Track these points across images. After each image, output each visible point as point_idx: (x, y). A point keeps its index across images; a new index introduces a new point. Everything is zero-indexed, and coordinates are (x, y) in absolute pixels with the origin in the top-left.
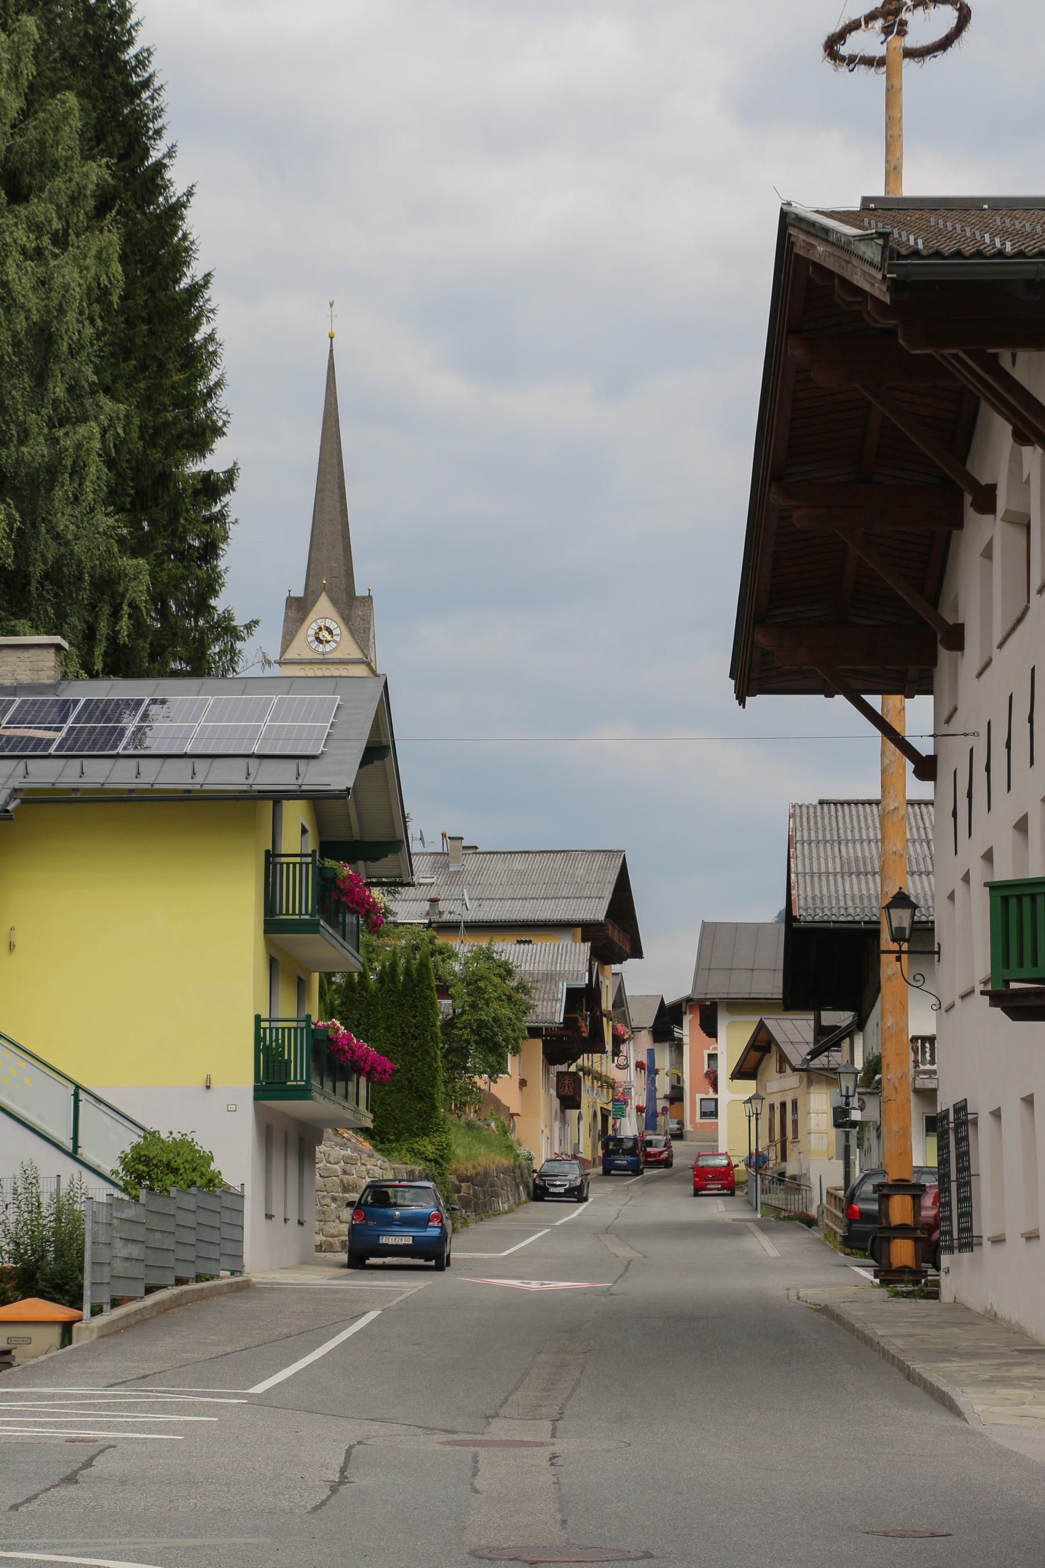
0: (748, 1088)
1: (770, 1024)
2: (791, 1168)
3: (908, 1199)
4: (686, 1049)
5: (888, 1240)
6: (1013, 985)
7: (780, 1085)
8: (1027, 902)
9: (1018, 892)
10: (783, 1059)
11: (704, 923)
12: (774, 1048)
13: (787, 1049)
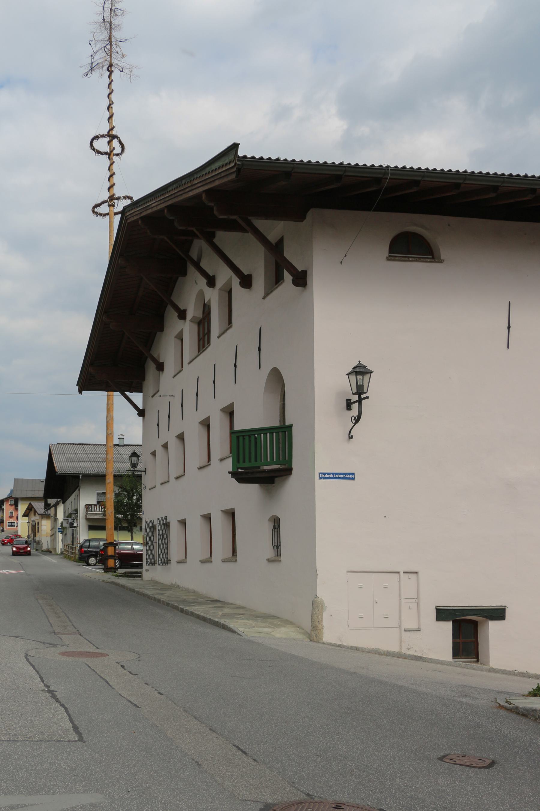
0: (26, 519)
1: (32, 503)
2: (37, 539)
3: (113, 548)
4: (5, 511)
5: (107, 559)
6: (239, 470)
7: (33, 517)
8: (247, 438)
9: (243, 434)
10: (35, 512)
11: (15, 479)
12: (33, 509)
13: (37, 510)
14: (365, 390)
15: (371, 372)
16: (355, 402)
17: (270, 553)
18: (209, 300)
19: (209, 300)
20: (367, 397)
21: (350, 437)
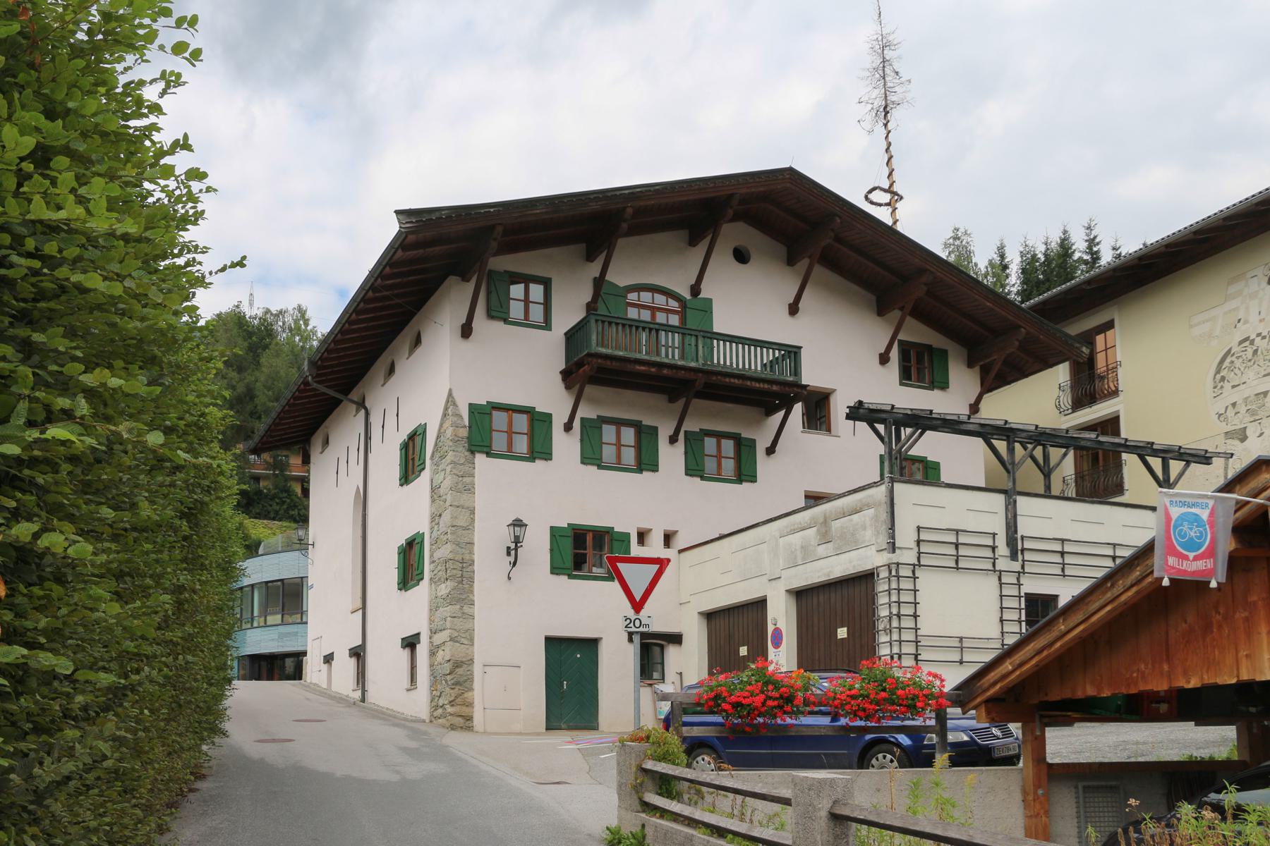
17: (406, 682)
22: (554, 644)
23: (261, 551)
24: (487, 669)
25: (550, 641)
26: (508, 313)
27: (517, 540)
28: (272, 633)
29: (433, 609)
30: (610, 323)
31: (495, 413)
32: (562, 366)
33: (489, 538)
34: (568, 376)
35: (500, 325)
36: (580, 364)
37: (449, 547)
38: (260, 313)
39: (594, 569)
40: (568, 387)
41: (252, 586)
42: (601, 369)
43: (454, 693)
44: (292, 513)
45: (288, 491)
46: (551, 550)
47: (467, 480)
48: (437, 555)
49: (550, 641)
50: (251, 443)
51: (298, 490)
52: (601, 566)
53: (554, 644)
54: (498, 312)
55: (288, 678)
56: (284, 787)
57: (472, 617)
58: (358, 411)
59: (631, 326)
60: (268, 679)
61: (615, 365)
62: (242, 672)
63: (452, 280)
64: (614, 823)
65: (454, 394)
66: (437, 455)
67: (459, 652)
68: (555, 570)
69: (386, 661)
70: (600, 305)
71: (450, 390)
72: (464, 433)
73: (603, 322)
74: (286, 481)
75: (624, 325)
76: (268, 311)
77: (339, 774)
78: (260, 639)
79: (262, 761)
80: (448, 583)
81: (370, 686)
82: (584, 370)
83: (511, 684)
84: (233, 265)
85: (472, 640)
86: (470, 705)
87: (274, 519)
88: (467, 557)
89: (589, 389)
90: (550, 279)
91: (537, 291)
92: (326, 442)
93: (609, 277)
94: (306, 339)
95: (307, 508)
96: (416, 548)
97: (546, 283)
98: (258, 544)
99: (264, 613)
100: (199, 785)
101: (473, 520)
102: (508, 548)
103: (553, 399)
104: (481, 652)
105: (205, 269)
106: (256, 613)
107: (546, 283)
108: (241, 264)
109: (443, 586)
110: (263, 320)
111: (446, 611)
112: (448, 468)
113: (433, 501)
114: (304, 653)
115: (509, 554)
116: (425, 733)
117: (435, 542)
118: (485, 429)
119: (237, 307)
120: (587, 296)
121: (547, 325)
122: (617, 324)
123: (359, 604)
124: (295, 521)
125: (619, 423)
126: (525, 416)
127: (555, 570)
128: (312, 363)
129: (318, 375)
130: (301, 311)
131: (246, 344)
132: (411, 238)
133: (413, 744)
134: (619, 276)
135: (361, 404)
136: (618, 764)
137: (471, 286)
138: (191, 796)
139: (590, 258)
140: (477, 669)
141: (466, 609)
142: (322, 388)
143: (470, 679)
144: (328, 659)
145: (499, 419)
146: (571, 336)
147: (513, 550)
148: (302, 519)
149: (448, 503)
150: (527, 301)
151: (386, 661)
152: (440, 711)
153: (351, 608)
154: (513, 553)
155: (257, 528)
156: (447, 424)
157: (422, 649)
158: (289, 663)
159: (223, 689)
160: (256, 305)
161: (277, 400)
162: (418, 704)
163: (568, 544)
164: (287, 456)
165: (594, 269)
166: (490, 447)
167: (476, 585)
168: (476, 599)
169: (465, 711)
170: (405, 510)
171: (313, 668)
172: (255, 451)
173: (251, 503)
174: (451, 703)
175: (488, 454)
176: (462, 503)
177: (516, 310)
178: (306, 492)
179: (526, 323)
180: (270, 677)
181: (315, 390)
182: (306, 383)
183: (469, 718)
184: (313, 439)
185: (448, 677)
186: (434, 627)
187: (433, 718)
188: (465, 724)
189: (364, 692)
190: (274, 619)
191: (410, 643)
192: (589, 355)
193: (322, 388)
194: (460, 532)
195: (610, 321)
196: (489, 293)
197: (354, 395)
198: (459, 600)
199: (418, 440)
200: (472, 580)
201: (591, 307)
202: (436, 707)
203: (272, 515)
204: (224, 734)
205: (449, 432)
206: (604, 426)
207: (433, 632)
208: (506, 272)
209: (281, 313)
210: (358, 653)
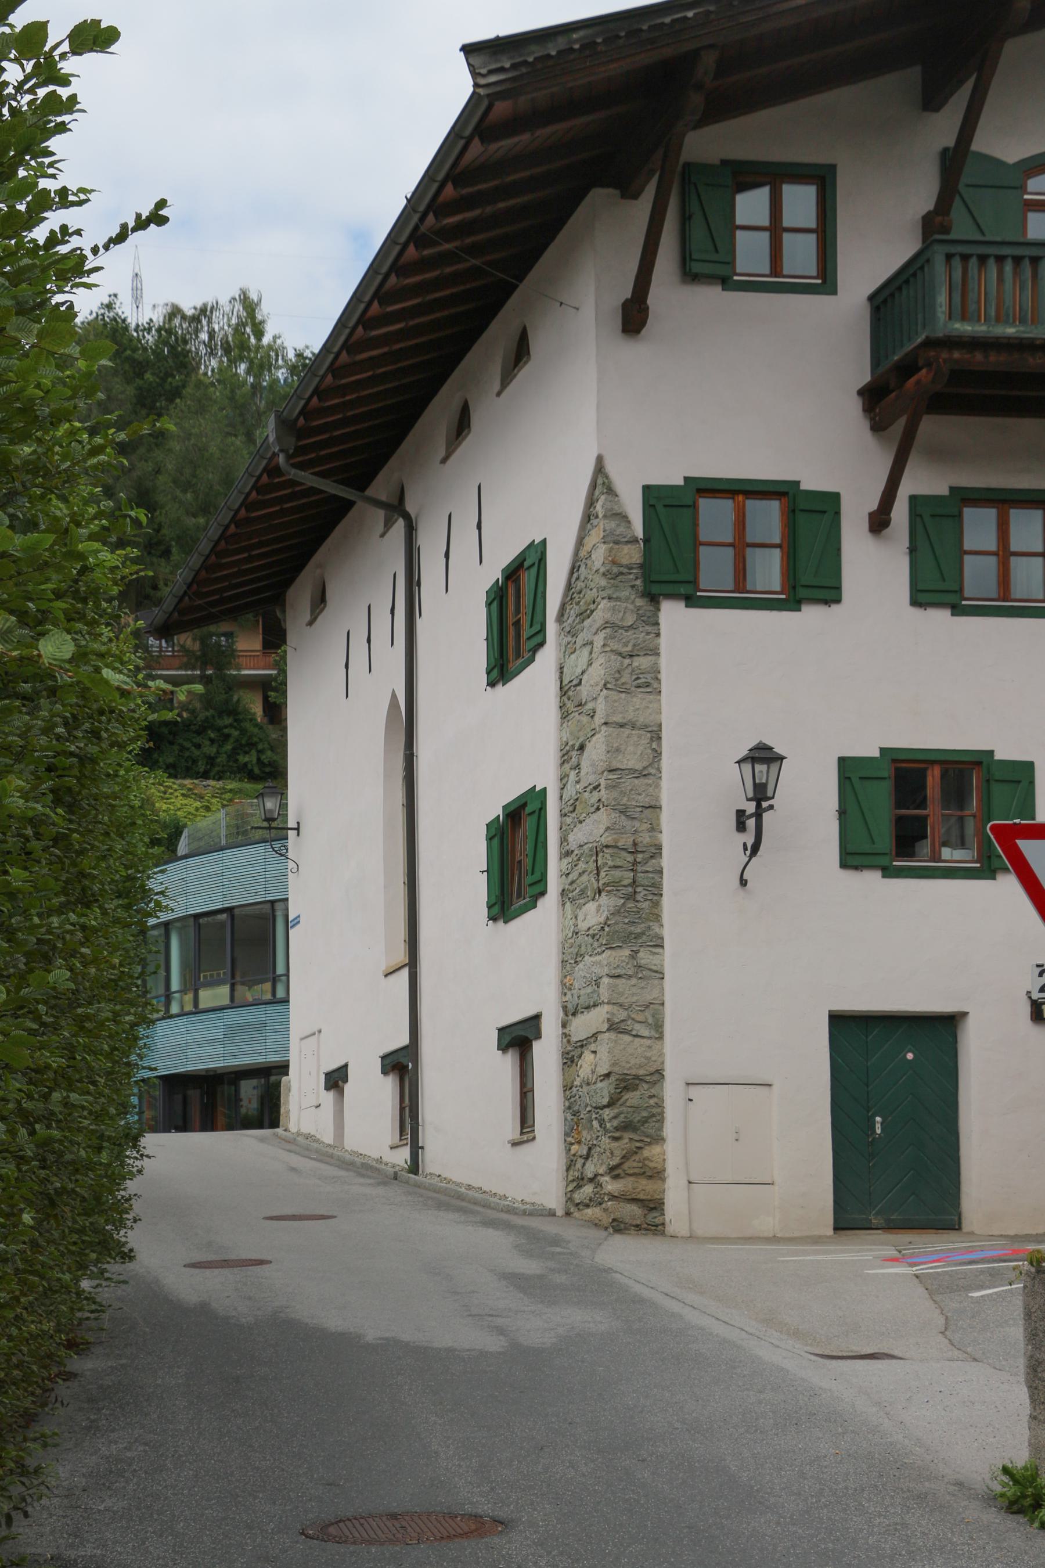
14: (770, 794)
15: (782, 758)
16: (751, 816)
17: (511, 1128)
18: (70, 130)
19: (70, 130)
20: (771, 807)
21: (743, 883)
22: (855, 1034)
23: (182, 848)
24: (694, 1092)
25: (839, 1021)
26: (732, 263)
27: (761, 794)
28: (211, 1027)
29: (570, 958)
30: (983, 259)
31: (703, 503)
32: (860, 372)
33: (693, 793)
34: (875, 398)
35: (711, 295)
36: (907, 368)
37: (603, 817)
38: (158, 317)
39: (946, 853)
40: (878, 427)
41: (167, 925)
42: (958, 375)
43: (619, 1148)
44: (243, 759)
45: (234, 712)
46: (842, 813)
47: (642, 662)
48: (577, 837)
49: (839, 1021)
50: (158, 614)
51: (257, 709)
52: (962, 844)
53: (855, 1034)
54: (709, 265)
55: (247, 1124)
56: (261, 1366)
57: (660, 975)
58: (388, 524)
59: (1017, 260)
60: (204, 1129)
61: (995, 360)
62: (148, 1114)
63: (598, 195)
64: (1020, 1457)
65: (610, 468)
66: (573, 611)
67: (631, 1053)
68: (852, 858)
69: (466, 1083)
70: (958, 213)
71: (600, 460)
72: (633, 555)
73: (965, 258)
74: (229, 689)
75: (1017, 260)
76: (175, 312)
77: (371, 1335)
78: (184, 1042)
79: (203, 1309)
80: (604, 899)
81: (428, 1137)
82: (916, 383)
83: (750, 1127)
84: (142, 224)
85: (658, 1027)
86: (658, 1174)
87: (205, 775)
88: (645, 839)
89: (930, 426)
90: (832, 168)
91: (800, 203)
92: (320, 600)
93: (980, 144)
94: (262, 364)
95: (281, 746)
96: (529, 824)
97: (823, 179)
98: (176, 832)
99: (193, 984)
100: (75, 1363)
101: (657, 754)
102: (741, 813)
103: (828, 449)
104: (680, 1056)
105: (82, 244)
106: (175, 986)
107: (823, 179)
108: (157, 218)
109: (591, 906)
110: (165, 331)
111: (599, 963)
112: (599, 641)
113: (565, 715)
114: (283, 1068)
115: (741, 827)
116: (556, 1241)
117: (571, 809)
118: (684, 545)
119: (109, 306)
120: (921, 195)
121: (826, 281)
122: (1000, 259)
123: (401, 955)
124: (253, 777)
125: (1004, 501)
126: (774, 507)
127: (852, 858)
128: (285, 425)
129: (300, 450)
130: (249, 305)
131: (131, 391)
132: (502, 108)
133: (530, 1267)
134: (1003, 142)
135: (396, 508)
136: (1028, 1315)
137: (642, 208)
138: (63, 1389)
139: (931, 100)
140: (672, 1092)
141: (645, 957)
142: (308, 479)
143: (657, 1116)
144: (336, 1079)
145: (715, 518)
146: (884, 303)
147: (753, 817)
148: (271, 773)
149: (599, 719)
150: (776, 229)
151: (466, 1083)
152: (588, 1189)
153: (383, 967)
154: (751, 823)
155: (171, 798)
156: (595, 537)
157: (546, 1053)
158: (249, 1091)
159: (120, 1157)
160: (148, 300)
161: (205, 509)
162: (537, 1175)
163: (881, 800)
164: (229, 635)
165: (942, 129)
166: (694, 582)
167: (666, 901)
168: (667, 933)
169: (645, 1187)
170: (501, 740)
171: (303, 1101)
172: (165, 630)
173: (171, 747)
174: (615, 1172)
175: (691, 601)
176: (630, 715)
177: (750, 253)
178: (276, 713)
179: (776, 282)
180: (209, 1124)
181: (293, 483)
182: (273, 470)
183: (655, 1205)
184: (291, 592)
185: (607, 1113)
186: (571, 999)
187: (573, 1206)
188: (647, 1216)
189: (416, 1149)
190: (215, 995)
191: (518, 1039)
192: (930, 343)
193: (308, 479)
194: (628, 782)
195: (982, 255)
196: (685, 219)
197: (381, 488)
198: (628, 938)
199: (527, 579)
200: (656, 890)
201: (933, 226)
202: (580, 1182)
203: (201, 767)
204: (128, 1256)
205: (599, 557)
206: (968, 512)
207: (570, 1012)
208: (725, 163)
209: (204, 312)
210: (402, 1065)
